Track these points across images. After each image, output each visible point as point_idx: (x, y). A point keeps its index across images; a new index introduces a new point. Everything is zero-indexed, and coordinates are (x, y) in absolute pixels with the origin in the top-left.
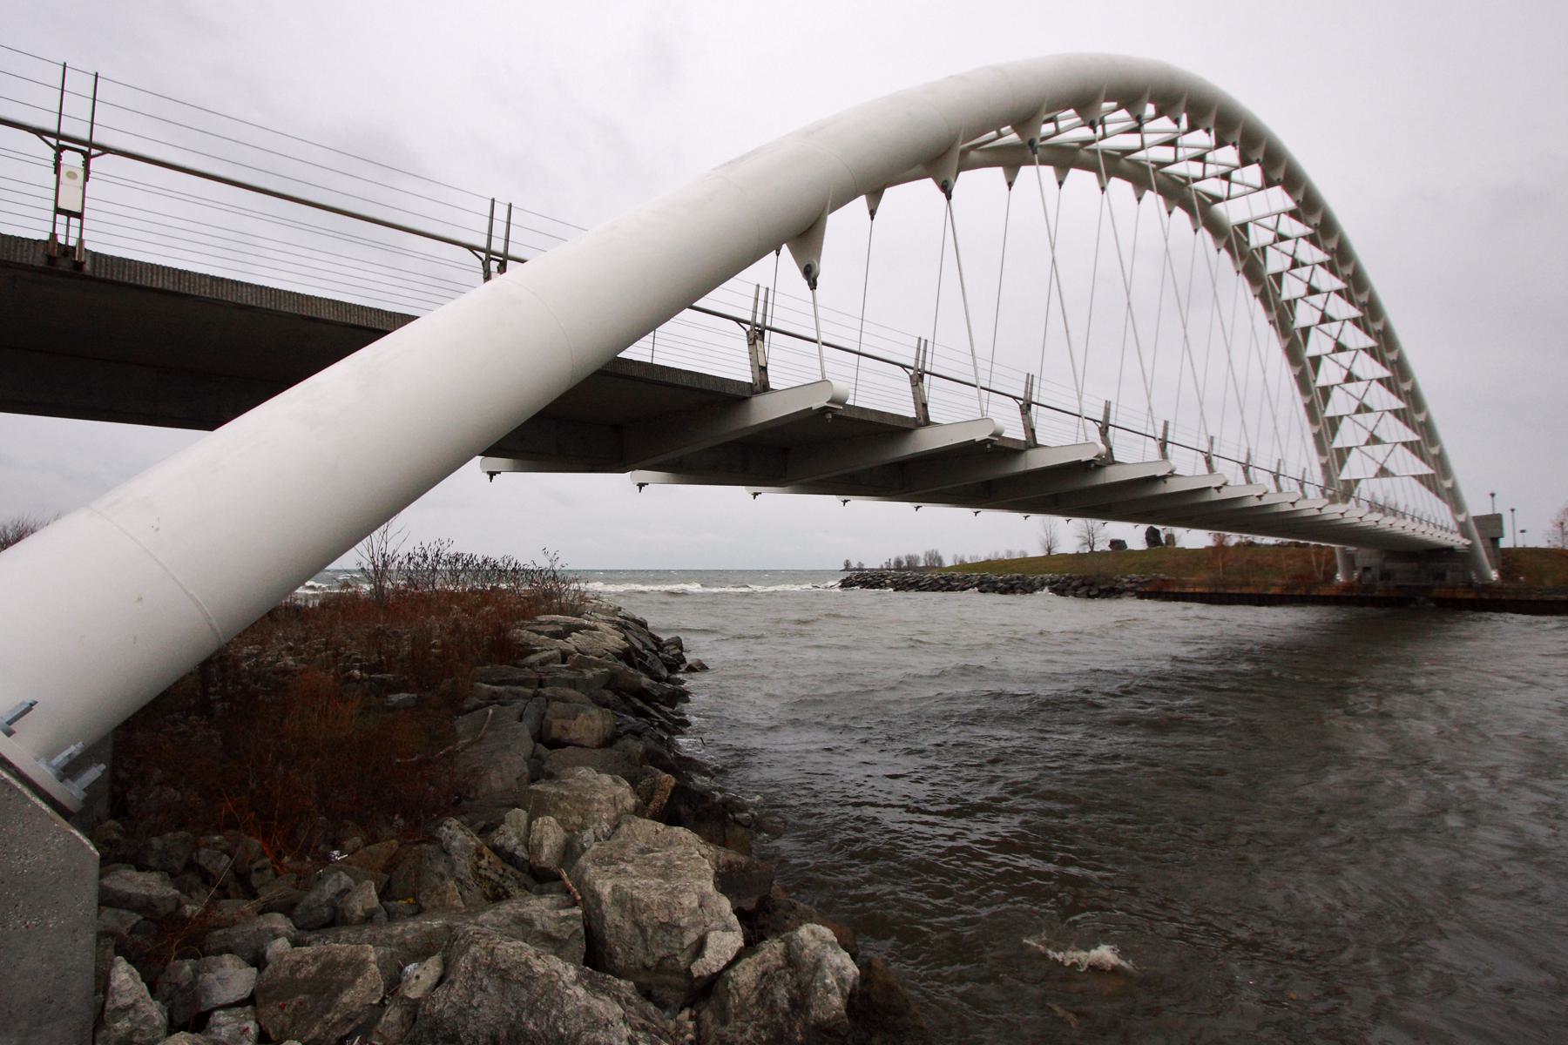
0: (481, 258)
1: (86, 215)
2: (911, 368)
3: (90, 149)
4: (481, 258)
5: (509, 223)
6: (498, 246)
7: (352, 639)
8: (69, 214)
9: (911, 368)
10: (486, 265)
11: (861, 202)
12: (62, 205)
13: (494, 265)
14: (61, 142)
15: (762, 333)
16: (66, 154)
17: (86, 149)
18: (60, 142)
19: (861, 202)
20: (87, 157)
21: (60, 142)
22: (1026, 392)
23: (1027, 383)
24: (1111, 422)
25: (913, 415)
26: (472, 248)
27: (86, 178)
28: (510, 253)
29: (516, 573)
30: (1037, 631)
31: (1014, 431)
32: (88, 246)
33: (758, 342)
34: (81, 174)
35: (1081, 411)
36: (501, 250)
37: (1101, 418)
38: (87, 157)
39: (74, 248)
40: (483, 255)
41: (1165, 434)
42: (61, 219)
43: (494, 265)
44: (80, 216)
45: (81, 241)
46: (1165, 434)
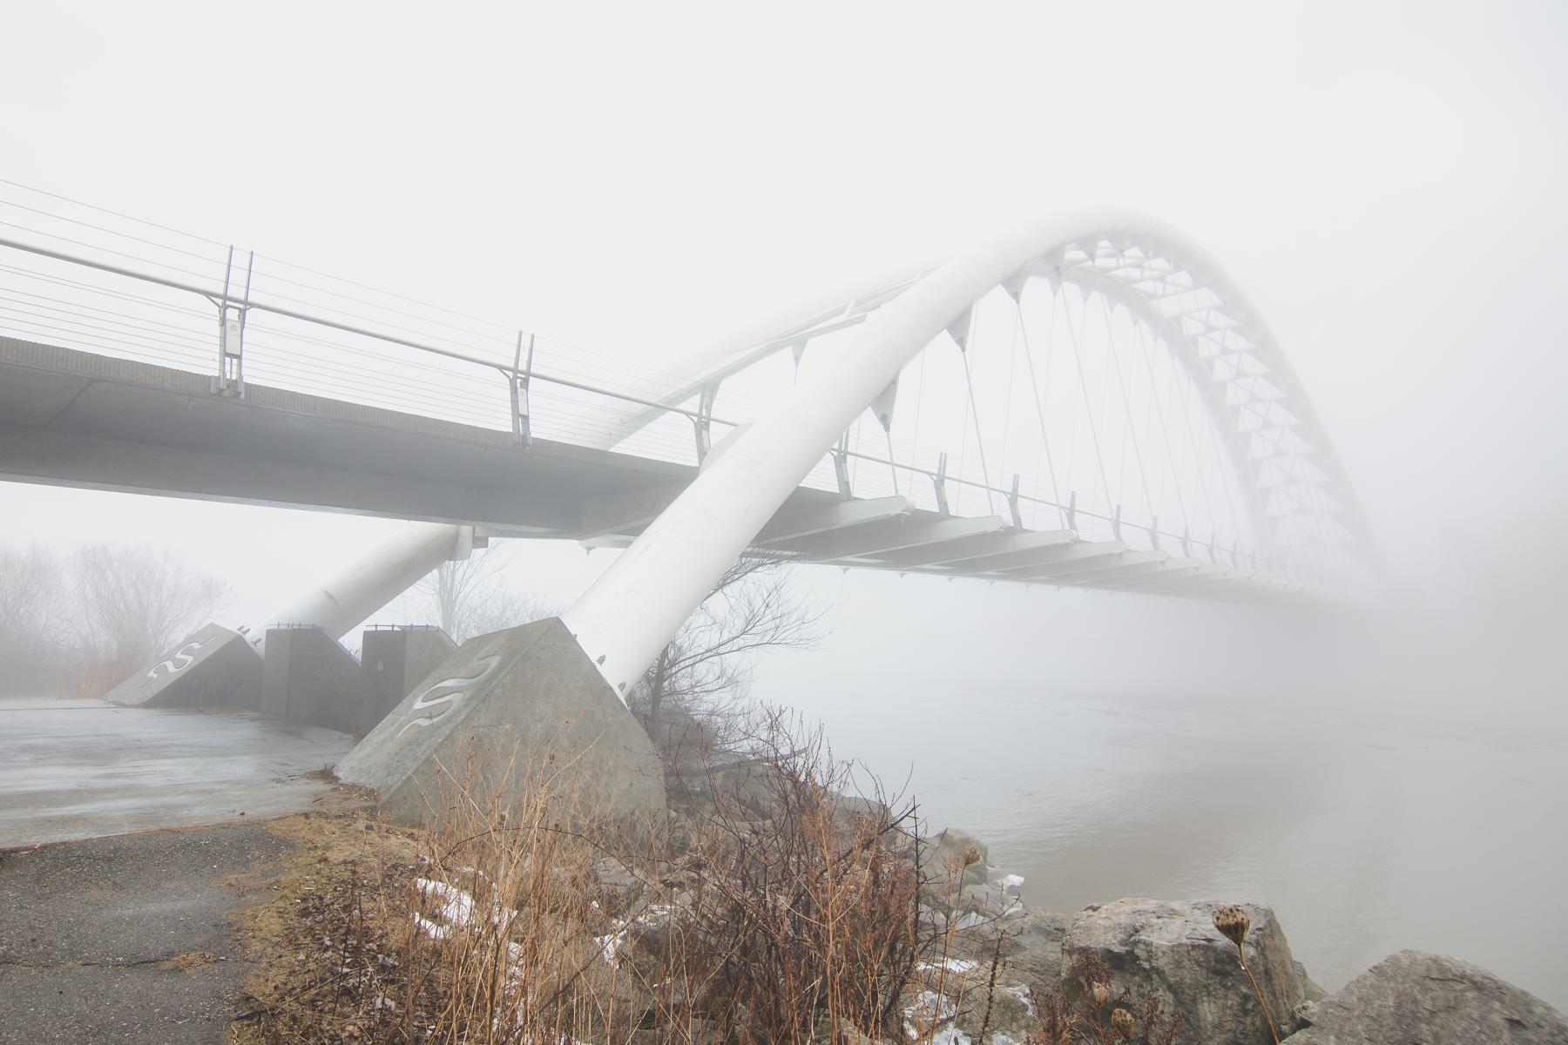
0: (508, 376)
1: (244, 355)
2: (510, 370)
3: (246, 305)
4: (508, 376)
5: (229, 265)
6: (236, 291)
7: (359, 987)
8: (232, 356)
9: (510, 370)
10: (512, 382)
11: (788, 352)
12: (229, 350)
13: (232, 314)
14: (228, 303)
15: (707, 424)
16: (229, 311)
17: (241, 306)
18: (224, 301)
19: (788, 352)
20: (243, 313)
21: (224, 301)
22: (940, 468)
23: (940, 461)
24: (1121, 520)
25: (837, 490)
26: (208, 294)
27: (243, 327)
28: (533, 370)
29: (1040, 582)
30: (1246, 903)
31: (928, 504)
32: (246, 380)
33: (704, 432)
34: (239, 325)
35: (1057, 501)
36: (242, 297)
37: (1068, 506)
38: (243, 313)
39: (235, 381)
40: (220, 301)
41: (1015, 489)
42: (228, 360)
43: (232, 314)
44: (239, 357)
45: (241, 377)
46: (1015, 489)
